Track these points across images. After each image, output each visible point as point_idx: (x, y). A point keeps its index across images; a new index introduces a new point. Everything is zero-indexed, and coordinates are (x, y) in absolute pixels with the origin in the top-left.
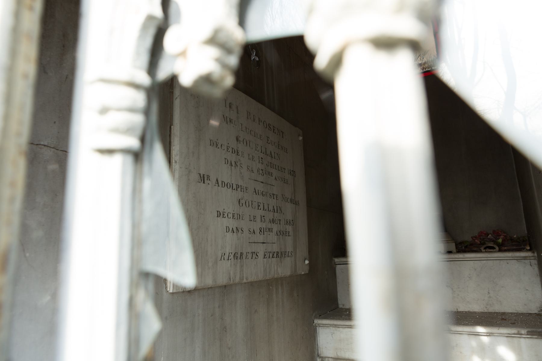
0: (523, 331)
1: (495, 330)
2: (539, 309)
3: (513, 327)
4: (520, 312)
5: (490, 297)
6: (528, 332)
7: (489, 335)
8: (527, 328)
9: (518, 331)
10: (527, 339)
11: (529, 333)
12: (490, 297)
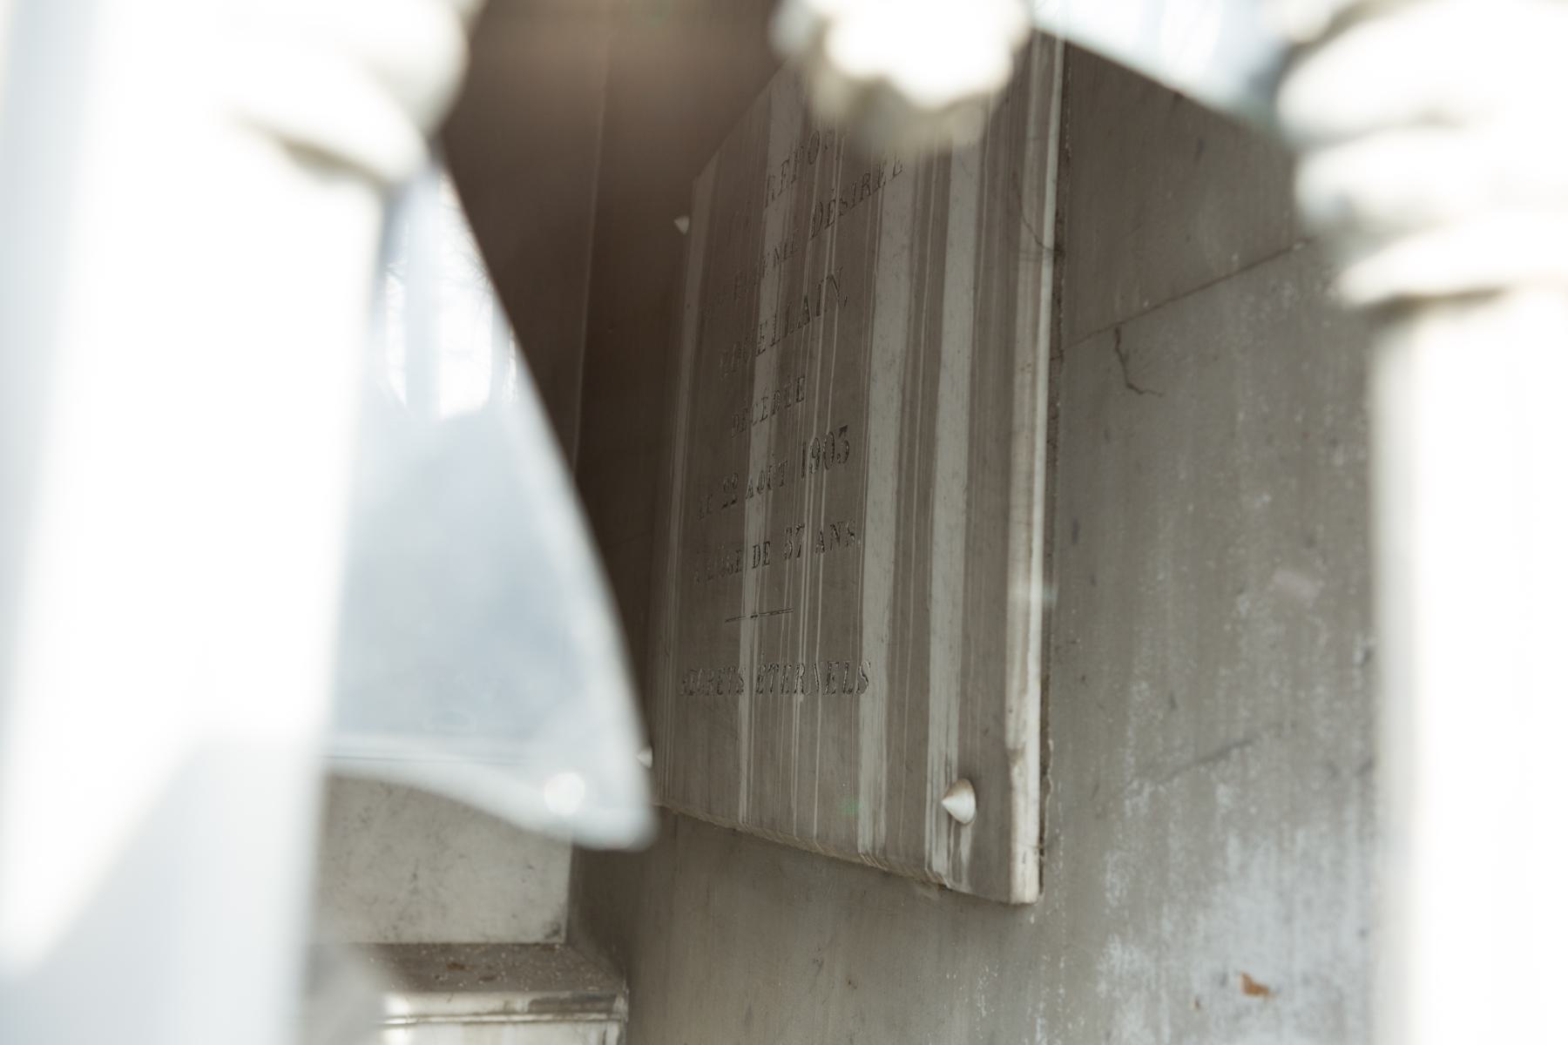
0: (521, 1002)
1: (438, 1004)
2: (548, 930)
3: (491, 990)
4: (494, 941)
5: (415, 891)
6: (533, 1003)
7: (419, 1021)
8: (532, 989)
9: (507, 1003)
10: (521, 1027)
11: (538, 1008)
12: (415, 891)
